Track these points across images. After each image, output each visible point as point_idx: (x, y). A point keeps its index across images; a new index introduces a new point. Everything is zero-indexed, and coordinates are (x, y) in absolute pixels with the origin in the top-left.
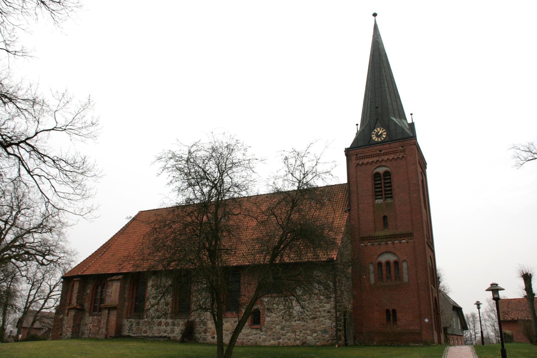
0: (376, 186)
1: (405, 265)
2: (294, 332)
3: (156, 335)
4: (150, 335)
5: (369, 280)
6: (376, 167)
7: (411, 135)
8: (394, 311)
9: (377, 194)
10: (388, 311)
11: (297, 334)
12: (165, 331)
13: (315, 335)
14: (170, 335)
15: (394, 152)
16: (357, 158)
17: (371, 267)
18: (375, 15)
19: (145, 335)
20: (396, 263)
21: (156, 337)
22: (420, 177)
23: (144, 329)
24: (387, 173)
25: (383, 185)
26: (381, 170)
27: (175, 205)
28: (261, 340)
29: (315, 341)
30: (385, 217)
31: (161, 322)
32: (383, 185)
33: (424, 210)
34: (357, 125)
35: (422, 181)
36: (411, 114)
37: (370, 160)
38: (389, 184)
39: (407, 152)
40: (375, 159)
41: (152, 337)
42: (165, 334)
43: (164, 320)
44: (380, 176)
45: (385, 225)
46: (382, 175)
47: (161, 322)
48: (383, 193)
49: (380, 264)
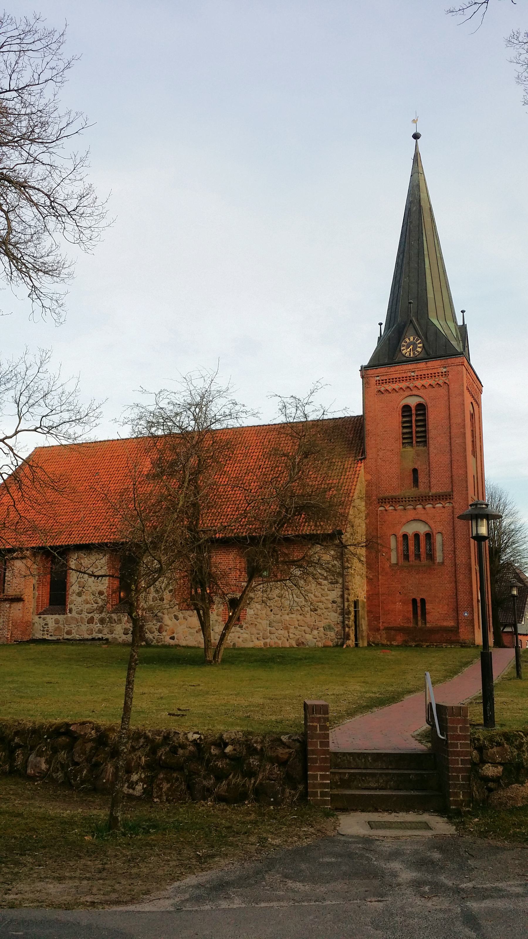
0: (406, 424)
1: (438, 539)
2: (287, 628)
3: (87, 636)
4: (77, 637)
5: (389, 559)
6: (405, 396)
7: (459, 349)
8: (423, 601)
9: (407, 439)
10: (414, 601)
11: (291, 631)
12: (100, 631)
13: (315, 632)
14: (109, 636)
15: (432, 376)
16: (378, 383)
17: (393, 543)
18: (416, 136)
19: (69, 637)
20: (428, 536)
21: (87, 640)
22: (468, 409)
23: (67, 628)
24: (421, 407)
25: (415, 423)
26: (413, 402)
27: (352, 814)
28: (240, 640)
29: (315, 640)
30: (415, 471)
31: (92, 618)
32: (415, 423)
33: (470, 459)
34: (381, 324)
35: (472, 416)
36: (463, 312)
37: (396, 386)
38: (423, 423)
39: (450, 377)
40: (403, 385)
41: (80, 640)
42: (100, 636)
43: (97, 615)
44: (411, 410)
45: (416, 482)
46: (413, 409)
47: (92, 618)
48: (414, 435)
49: (405, 536)
